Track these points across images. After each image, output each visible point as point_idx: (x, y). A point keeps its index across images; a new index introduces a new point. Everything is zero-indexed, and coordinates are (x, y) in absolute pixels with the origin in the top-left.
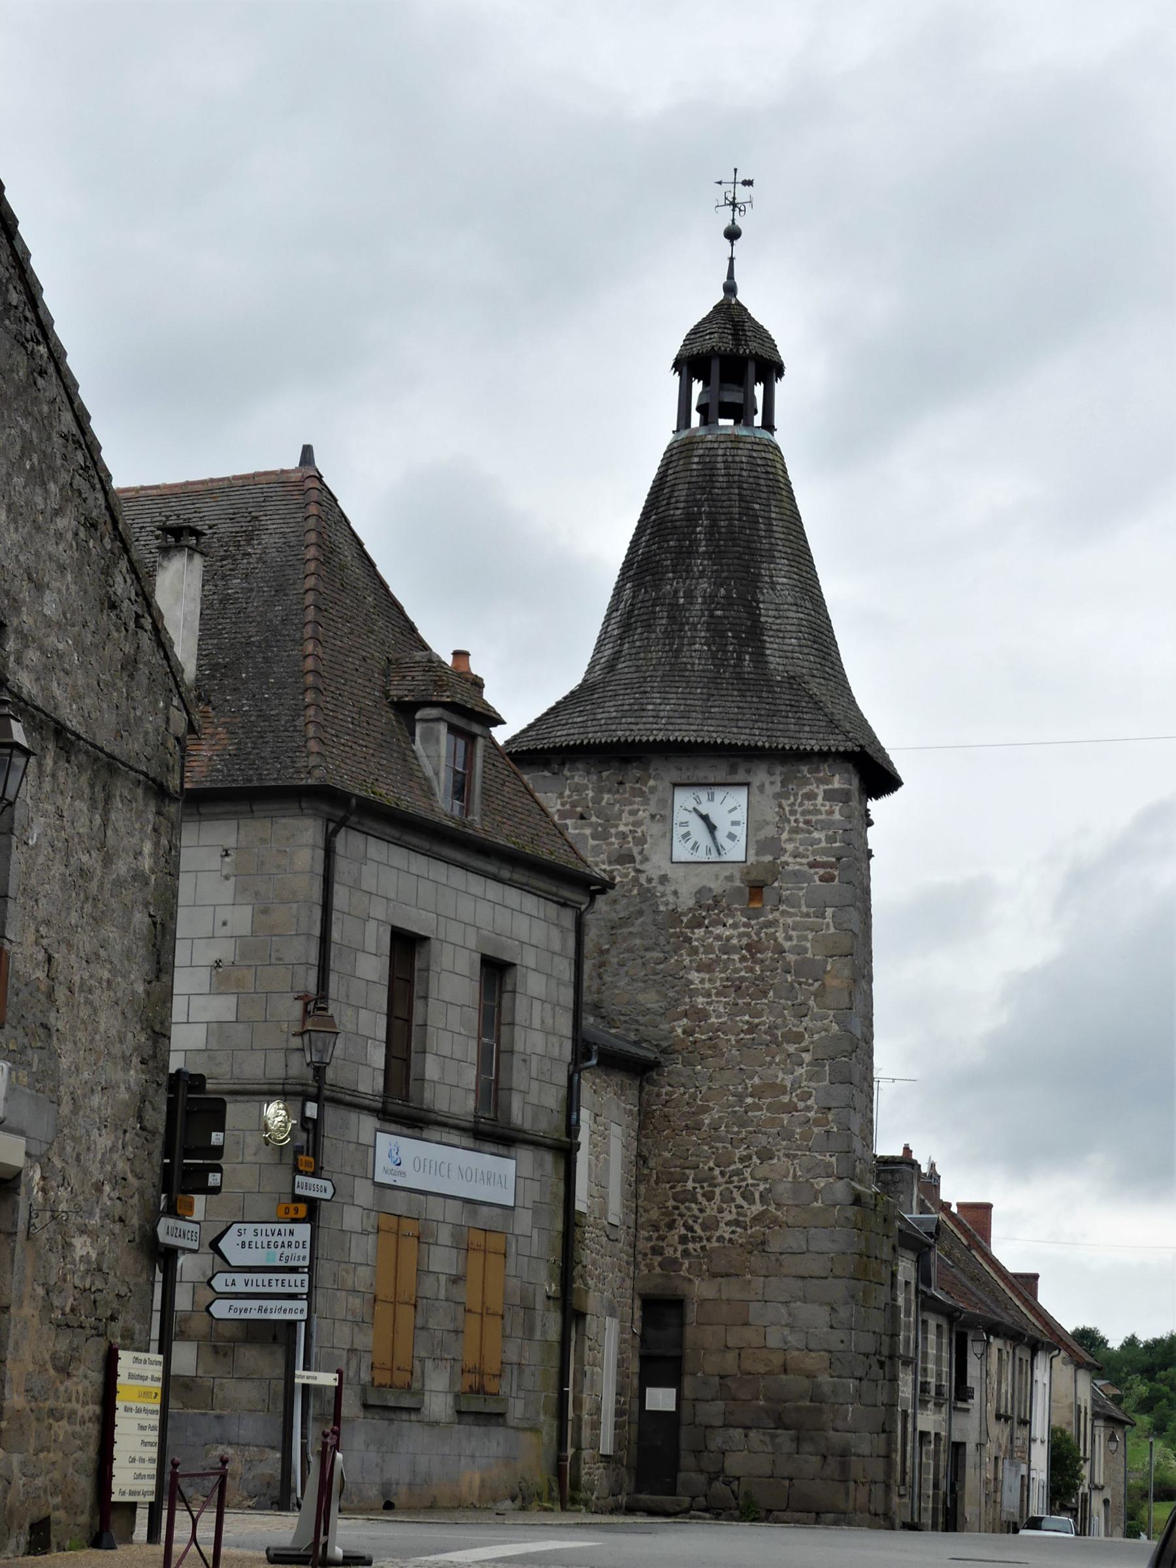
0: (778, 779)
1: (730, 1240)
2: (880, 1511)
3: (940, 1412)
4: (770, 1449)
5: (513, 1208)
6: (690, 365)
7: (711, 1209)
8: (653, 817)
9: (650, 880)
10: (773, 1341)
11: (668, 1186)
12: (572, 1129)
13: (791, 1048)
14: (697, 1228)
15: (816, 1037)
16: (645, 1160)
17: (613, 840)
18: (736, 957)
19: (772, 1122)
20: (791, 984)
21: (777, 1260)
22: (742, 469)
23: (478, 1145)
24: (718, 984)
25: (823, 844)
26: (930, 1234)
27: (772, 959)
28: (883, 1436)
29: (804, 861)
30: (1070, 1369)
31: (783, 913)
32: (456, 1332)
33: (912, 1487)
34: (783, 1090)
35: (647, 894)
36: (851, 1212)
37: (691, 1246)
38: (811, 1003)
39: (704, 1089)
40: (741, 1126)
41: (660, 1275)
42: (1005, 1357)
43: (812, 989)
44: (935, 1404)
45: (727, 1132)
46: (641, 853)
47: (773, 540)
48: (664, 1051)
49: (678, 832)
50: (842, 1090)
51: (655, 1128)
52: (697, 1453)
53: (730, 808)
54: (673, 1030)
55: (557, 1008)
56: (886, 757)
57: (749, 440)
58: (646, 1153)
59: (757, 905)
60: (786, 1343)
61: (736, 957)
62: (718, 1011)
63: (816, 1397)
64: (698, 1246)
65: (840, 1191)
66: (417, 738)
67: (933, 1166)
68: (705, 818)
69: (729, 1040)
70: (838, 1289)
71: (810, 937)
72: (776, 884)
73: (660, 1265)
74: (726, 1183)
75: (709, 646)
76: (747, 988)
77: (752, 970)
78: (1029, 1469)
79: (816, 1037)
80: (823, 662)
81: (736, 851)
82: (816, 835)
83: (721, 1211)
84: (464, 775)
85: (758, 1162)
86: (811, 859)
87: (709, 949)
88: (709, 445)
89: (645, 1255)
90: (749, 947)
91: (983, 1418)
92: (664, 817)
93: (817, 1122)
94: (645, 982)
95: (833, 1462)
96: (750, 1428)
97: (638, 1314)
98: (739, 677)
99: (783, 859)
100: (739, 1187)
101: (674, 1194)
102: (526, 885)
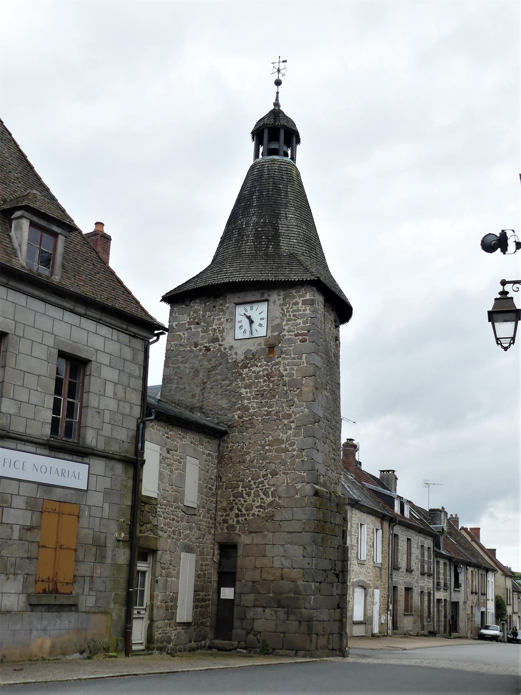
0: (281, 297)
1: (258, 515)
2: (336, 647)
3: (446, 592)
5: (86, 491)
6: (258, 134)
7: (249, 500)
8: (227, 320)
9: (225, 349)
10: (277, 564)
11: (231, 490)
12: (139, 452)
13: (286, 421)
14: (243, 510)
15: (298, 415)
16: (221, 478)
17: (210, 332)
18: (261, 380)
19: (277, 457)
20: (286, 391)
21: (279, 524)
22: (275, 172)
23: (53, 453)
24: (254, 393)
25: (302, 325)
26: (439, 532)
27: (278, 380)
28: (339, 610)
29: (293, 333)
30: (503, 577)
31: (284, 358)
32: (30, 558)
33: (433, 618)
34: (282, 442)
35: (224, 356)
36: (313, 499)
37: (240, 518)
38: (296, 399)
39: (247, 443)
40: (263, 460)
41: (227, 533)
42: (474, 573)
43: (296, 393)
44: (444, 589)
45: (257, 463)
46: (222, 337)
47: (288, 200)
48: (229, 427)
49: (238, 325)
50: (310, 440)
51: (225, 463)
52: (242, 620)
53: (259, 312)
54: (234, 416)
55: (128, 389)
56: (341, 291)
57: (280, 161)
58: (221, 475)
59: (271, 356)
60: (282, 565)
61: (261, 380)
62: (253, 406)
63: (297, 592)
64: (243, 518)
65: (308, 489)
66: (13, 229)
67: (456, 515)
68: (249, 318)
69: (258, 420)
70: (307, 537)
71: (295, 369)
72: (280, 345)
73: (227, 528)
74: (257, 488)
75: (254, 243)
76: (266, 394)
77: (268, 386)
78: (487, 609)
79: (298, 415)
80: (310, 251)
81: (261, 332)
82: (298, 321)
83: (254, 501)
84: (51, 254)
85: (271, 477)
86: (296, 332)
87: (250, 378)
88: (262, 164)
89: (220, 523)
90: (267, 375)
92: (232, 320)
93: (298, 457)
94: (222, 395)
95: (304, 625)
96: (265, 607)
97: (217, 552)
98: (266, 254)
99: (283, 333)
100: (262, 490)
101: (233, 494)
102: (100, 320)
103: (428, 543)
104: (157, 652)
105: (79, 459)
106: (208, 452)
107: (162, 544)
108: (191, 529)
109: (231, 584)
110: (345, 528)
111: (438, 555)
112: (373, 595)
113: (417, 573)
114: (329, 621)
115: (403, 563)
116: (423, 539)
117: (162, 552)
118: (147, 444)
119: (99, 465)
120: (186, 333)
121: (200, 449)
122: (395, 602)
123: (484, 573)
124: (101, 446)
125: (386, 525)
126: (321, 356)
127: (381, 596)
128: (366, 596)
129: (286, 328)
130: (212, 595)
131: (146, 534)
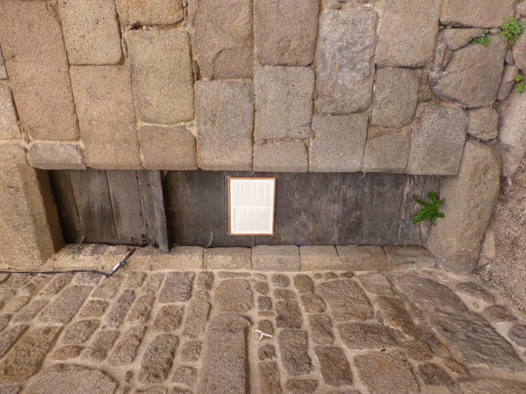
109: (213, 182)
130: (266, 265)
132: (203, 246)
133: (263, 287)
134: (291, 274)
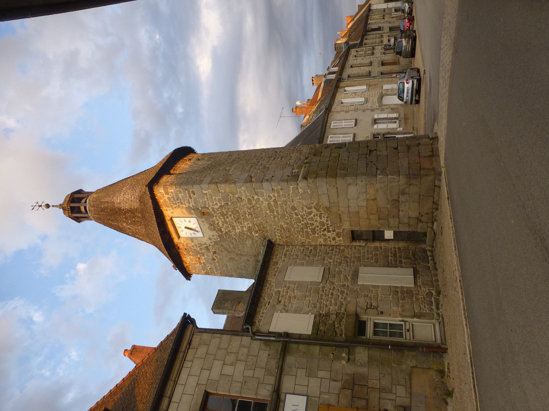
4: (408, 203)
5: (308, 396)
13: (254, 202)
14: (324, 228)
18: (228, 220)
19: (282, 207)
31: (209, 205)
34: (269, 204)
35: (216, 243)
37: (331, 229)
38: (237, 196)
39: (275, 227)
40: (285, 216)
62: (247, 224)
64: (331, 227)
70: (340, 182)
77: (230, 215)
82: (181, 197)
87: (227, 227)
91: (384, 23)
93: (278, 193)
102: (175, 381)
103: (353, 52)
104: (441, 310)
105: (281, 404)
106: (283, 256)
107: (351, 308)
108: (340, 272)
110: (334, 147)
111: (361, 44)
112: (387, 90)
113: (372, 58)
114: (408, 157)
115: (367, 69)
116: (351, 56)
117: (358, 308)
118: (272, 330)
119: (287, 383)
120: (207, 265)
121: (280, 265)
122: (391, 73)
123: (371, 12)
124: (272, 380)
125: (342, 84)
126: (204, 177)
127: (388, 83)
128: (388, 95)
129: (187, 205)
130: (392, 245)
131: (343, 328)
132: (379, 240)
133: (391, 249)
134: (397, 247)
